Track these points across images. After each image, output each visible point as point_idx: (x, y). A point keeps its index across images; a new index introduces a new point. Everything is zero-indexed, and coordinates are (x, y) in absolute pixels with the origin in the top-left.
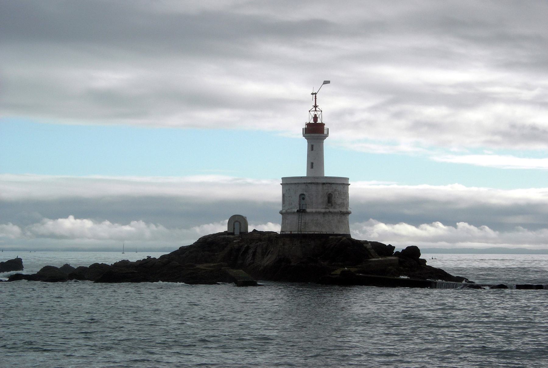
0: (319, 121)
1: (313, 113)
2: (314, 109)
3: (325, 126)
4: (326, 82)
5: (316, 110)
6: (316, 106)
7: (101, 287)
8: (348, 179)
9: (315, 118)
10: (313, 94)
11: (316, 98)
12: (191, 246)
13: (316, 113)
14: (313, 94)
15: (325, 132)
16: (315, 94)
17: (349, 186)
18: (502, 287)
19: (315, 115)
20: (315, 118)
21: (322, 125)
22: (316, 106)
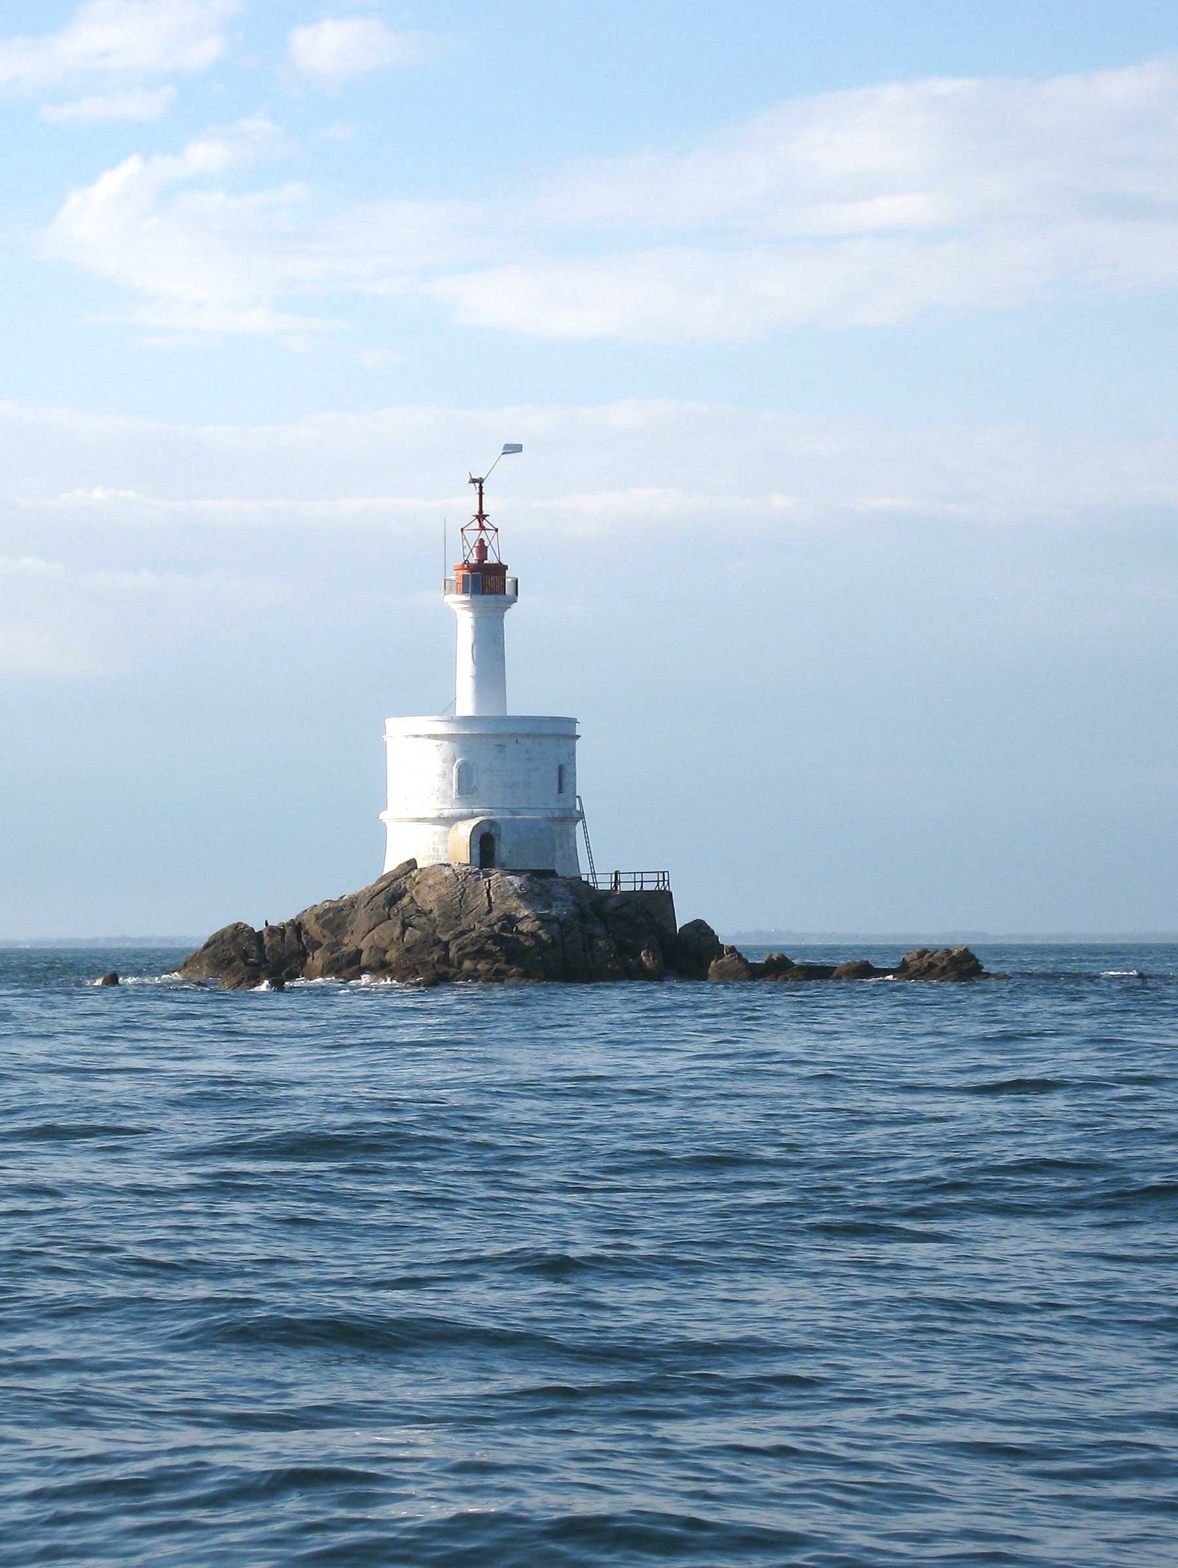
0: (491, 559)
1: (473, 537)
2: (476, 524)
3: (508, 573)
4: (513, 449)
5: (482, 528)
6: (481, 517)
7: (304, 1357)
8: (573, 722)
9: (482, 549)
10: (474, 481)
11: (481, 494)
12: (477, 619)
13: (483, 535)
14: (474, 481)
15: (509, 590)
16: (480, 481)
17: (578, 742)
18: (417, 736)
19: (482, 541)
20: (482, 549)
21: (500, 569)
22: (481, 517)
